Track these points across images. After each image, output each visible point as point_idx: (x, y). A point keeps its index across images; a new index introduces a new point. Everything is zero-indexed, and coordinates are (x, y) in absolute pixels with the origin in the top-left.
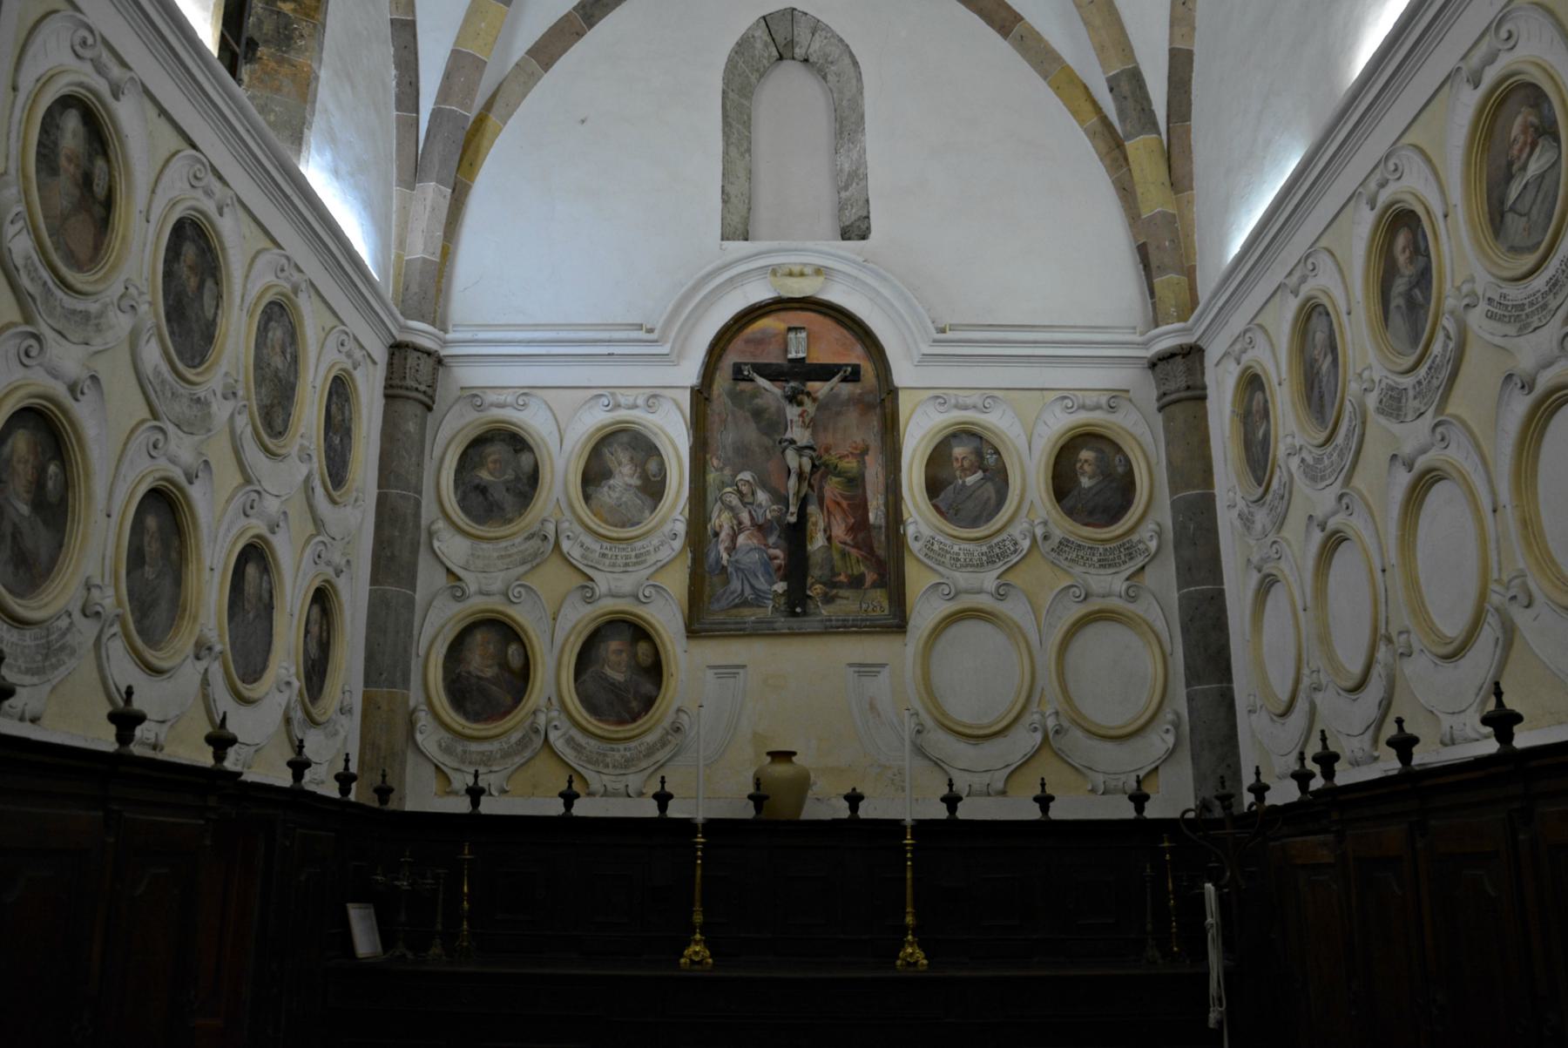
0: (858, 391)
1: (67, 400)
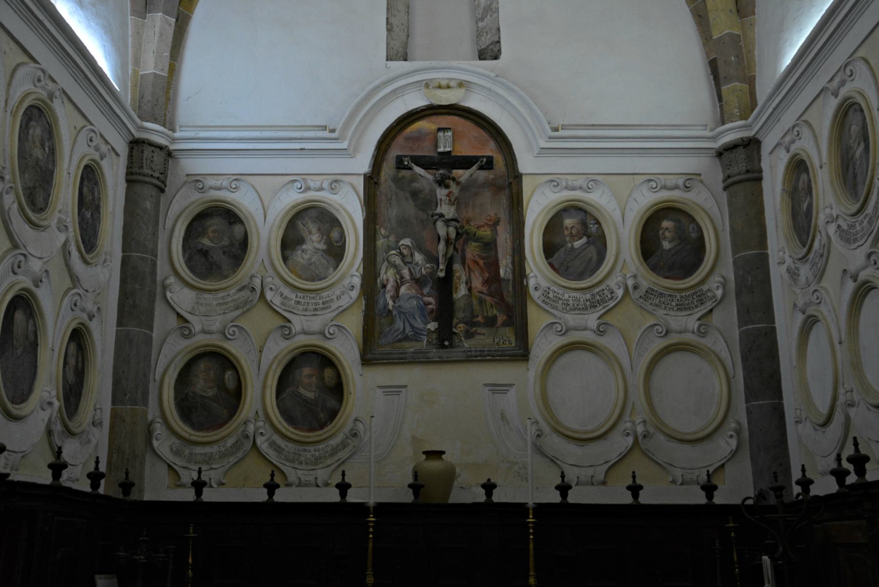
0: (492, 177)
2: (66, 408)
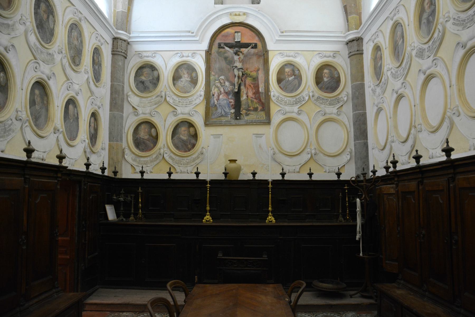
1: (4, 53)
2: (91, 143)
